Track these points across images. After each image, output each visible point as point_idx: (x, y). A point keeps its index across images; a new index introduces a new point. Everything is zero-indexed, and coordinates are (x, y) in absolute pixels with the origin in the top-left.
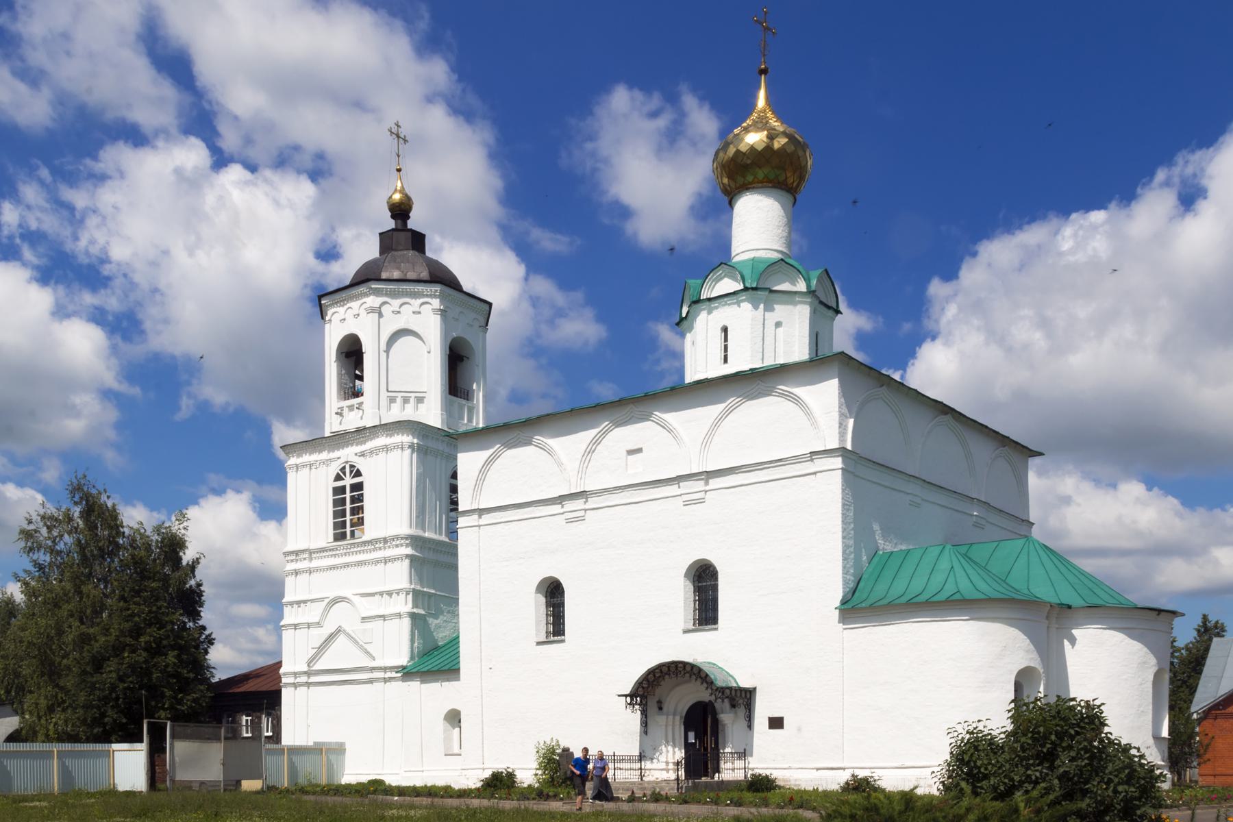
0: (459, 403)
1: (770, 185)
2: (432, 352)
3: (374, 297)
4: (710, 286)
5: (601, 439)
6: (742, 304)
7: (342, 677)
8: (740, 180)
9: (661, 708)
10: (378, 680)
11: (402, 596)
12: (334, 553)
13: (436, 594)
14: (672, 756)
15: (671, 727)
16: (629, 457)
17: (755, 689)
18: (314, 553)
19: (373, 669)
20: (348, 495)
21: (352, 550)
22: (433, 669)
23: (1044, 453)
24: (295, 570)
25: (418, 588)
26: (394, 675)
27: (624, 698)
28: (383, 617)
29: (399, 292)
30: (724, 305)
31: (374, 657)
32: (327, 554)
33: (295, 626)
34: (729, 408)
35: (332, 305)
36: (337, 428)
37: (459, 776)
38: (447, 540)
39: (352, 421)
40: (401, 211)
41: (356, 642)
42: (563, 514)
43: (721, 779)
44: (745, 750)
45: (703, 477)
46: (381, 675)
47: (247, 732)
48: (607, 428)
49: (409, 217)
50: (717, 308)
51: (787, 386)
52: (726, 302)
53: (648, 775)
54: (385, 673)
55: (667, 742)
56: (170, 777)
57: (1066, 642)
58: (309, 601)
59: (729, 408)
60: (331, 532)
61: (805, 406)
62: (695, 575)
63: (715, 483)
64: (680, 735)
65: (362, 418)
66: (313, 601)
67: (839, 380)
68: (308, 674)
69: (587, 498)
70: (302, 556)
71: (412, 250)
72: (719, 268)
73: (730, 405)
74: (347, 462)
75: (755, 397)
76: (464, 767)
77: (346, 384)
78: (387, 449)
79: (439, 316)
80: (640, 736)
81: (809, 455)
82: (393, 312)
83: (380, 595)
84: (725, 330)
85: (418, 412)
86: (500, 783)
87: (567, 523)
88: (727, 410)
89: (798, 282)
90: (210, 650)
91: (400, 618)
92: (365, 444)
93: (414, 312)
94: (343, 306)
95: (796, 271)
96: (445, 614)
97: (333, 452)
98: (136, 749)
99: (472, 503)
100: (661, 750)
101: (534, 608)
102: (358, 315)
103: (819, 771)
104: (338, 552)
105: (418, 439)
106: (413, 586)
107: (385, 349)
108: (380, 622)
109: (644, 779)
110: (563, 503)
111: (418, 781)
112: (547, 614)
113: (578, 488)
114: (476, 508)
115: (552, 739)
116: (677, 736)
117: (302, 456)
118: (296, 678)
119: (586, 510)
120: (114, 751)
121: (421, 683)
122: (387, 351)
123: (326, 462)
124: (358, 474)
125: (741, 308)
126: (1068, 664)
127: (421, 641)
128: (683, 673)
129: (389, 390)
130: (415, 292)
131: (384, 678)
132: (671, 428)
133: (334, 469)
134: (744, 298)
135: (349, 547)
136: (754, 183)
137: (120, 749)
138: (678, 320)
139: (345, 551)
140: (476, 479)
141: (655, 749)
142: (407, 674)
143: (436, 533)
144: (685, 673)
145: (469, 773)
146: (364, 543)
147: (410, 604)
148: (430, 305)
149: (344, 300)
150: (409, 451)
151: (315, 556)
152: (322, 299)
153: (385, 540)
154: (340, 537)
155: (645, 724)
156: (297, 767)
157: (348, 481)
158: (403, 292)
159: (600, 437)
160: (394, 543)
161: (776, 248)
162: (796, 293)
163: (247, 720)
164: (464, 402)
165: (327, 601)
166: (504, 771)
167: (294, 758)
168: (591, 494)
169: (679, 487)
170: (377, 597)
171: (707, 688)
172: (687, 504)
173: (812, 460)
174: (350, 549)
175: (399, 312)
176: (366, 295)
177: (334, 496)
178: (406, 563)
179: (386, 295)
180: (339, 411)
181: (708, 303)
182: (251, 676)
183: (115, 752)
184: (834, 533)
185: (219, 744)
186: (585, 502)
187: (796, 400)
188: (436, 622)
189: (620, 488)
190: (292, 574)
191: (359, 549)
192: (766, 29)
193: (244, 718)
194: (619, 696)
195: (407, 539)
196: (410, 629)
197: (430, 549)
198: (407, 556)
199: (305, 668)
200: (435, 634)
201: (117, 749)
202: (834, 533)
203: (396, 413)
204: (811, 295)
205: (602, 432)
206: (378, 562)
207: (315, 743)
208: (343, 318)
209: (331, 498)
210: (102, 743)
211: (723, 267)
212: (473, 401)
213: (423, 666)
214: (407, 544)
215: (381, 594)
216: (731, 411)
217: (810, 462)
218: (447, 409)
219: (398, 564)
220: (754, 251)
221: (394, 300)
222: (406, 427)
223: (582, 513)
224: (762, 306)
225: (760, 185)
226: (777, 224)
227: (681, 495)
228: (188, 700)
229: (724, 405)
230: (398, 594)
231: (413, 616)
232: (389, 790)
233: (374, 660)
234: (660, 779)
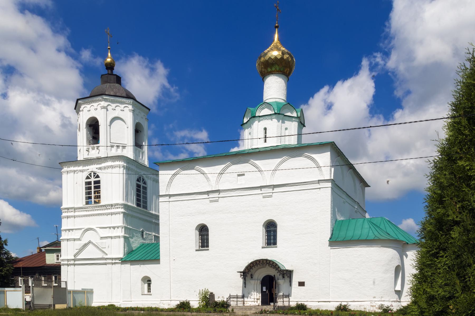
0: (139, 150)
1: (281, 73)
3: (105, 102)
4: (260, 111)
5: (226, 169)
6: (273, 119)
8: (269, 70)
9: (252, 278)
10: (109, 263)
11: (120, 229)
12: (86, 209)
13: (132, 229)
14: (256, 296)
15: (256, 285)
16: (238, 177)
17: (293, 271)
18: (76, 209)
20: (93, 185)
21: (95, 209)
23: (370, 186)
24: (67, 216)
25: (126, 226)
26: (117, 261)
27: (240, 273)
28: (111, 237)
29: (115, 101)
30: (265, 119)
32: (83, 210)
33: (68, 240)
34: (284, 160)
35: (84, 104)
36: (86, 156)
37: (160, 303)
38: (136, 206)
39: (94, 154)
41: (98, 247)
42: (209, 198)
43: (284, 305)
44: (289, 294)
45: (272, 187)
46: (110, 261)
47: (21, 284)
48: (229, 165)
50: (262, 120)
51: (308, 153)
52: (266, 118)
53: (246, 304)
54: (112, 260)
55: (254, 290)
56: (32, 302)
57: (404, 257)
58: (74, 229)
59: (284, 160)
60: (84, 201)
61: (316, 162)
62: (266, 226)
63: (276, 190)
64: (259, 289)
65: (99, 153)
67: (330, 153)
68: (74, 260)
69: (220, 193)
71: (117, 83)
72: (264, 104)
73: (284, 159)
74: (92, 172)
75: (295, 156)
76: (162, 300)
77: (89, 138)
78: (112, 167)
79: (132, 113)
80: (243, 288)
81: (318, 181)
82: (112, 109)
83: (109, 228)
84: (265, 129)
85: (123, 153)
86: (184, 306)
87: (210, 202)
88: (283, 161)
89: (294, 113)
91: (119, 238)
92: (101, 164)
93: (121, 110)
94: (89, 104)
95: (293, 108)
96: (135, 237)
97: (85, 166)
98: (17, 290)
100: (252, 293)
101: (194, 237)
102: (97, 109)
103: (319, 303)
104: (88, 209)
105: (126, 164)
106: (124, 225)
107: (109, 125)
108: (109, 240)
109: (245, 305)
110: (209, 194)
111: (128, 305)
112: (199, 239)
113: (216, 188)
114: (168, 194)
115: (205, 289)
116: (258, 289)
117: (70, 168)
118: (68, 262)
119: (219, 197)
120: (6, 291)
121: (131, 265)
122: (110, 126)
123: (82, 171)
124: (98, 177)
125: (273, 121)
126: (405, 264)
127: (128, 248)
128: (265, 264)
129: (111, 142)
130: (122, 101)
131: (112, 263)
132: (258, 166)
133: (86, 174)
134: (274, 117)
135: (90, 208)
136: (275, 71)
137: (9, 290)
138: (242, 124)
139: (92, 209)
140: (168, 182)
141: (249, 293)
142: (123, 261)
143: (132, 204)
144: (266, 264)
145: (164, 302)
146: (102, 206)
147: (123, 233)
148: (128, 108)
149: (89, 102)
150: (123, 168)
151: (77, 210)
152: (79, 100)
153: (112, 205)
154: (87, 203)
155: (245, 283)
156: (75, 299)
157: (93, 180)
158: (117, 101)
159: (226, 168)
160: (116, 207)
161: (282, 98)
162: (293, 117)
164: (140, 150)
166: (185, 301)
167: (75, 295)
168: (221, 191)
169: (261, 190)
170: (108, 229)
172: (264, 197)
173: (319, 183)
174: (94, 208)
175: (115, 110)
176: (100, 101)
177: (85, 185)
178: (122, 215)
179: (110, 102)
180: (87, 149)
181: (259, 118)
182: (17, 260)
183: (7, 292)
184: (327, 212)
186: (219, 194)
187: (313, 160)
188: (132, 240)
189: (235, 189)
190: (66, 218)
191: (99, 208)
192: (278, 10)
193: (20, 278)
194: (238, 272)
195: (122, 205)
196: (124, 243)
197: (130, 210)
198: (122, 212)
199: (73, 258)
200: (132, 245)
201: (8, 290)
202: (327, 212)
203: (114, 152)
204: (298, 119)
205: (227, 166)
206: (108, 214)
207: (82, 289)
208: (96, 108)
209: (84, 186)
210: (1, 288)
211: (265, 104)
212: (143, 149)
214: (122, 207)
215: (110, 228)
216: (284, 162)
217: (318, 184)
218: (135, 152)
220: (275, 99)
221: (113, 104)
222: (122, 158)
223: (217, 199)
224: (281, 121)
225: (277, 72)
226: (283, 89)
227: (262, 194)
228: (4, 270)
229: (281, 159)
230: (118, 228)
231: (125, 237)
232: (118, 309)
233: (107, 255)
234: (252, 305)
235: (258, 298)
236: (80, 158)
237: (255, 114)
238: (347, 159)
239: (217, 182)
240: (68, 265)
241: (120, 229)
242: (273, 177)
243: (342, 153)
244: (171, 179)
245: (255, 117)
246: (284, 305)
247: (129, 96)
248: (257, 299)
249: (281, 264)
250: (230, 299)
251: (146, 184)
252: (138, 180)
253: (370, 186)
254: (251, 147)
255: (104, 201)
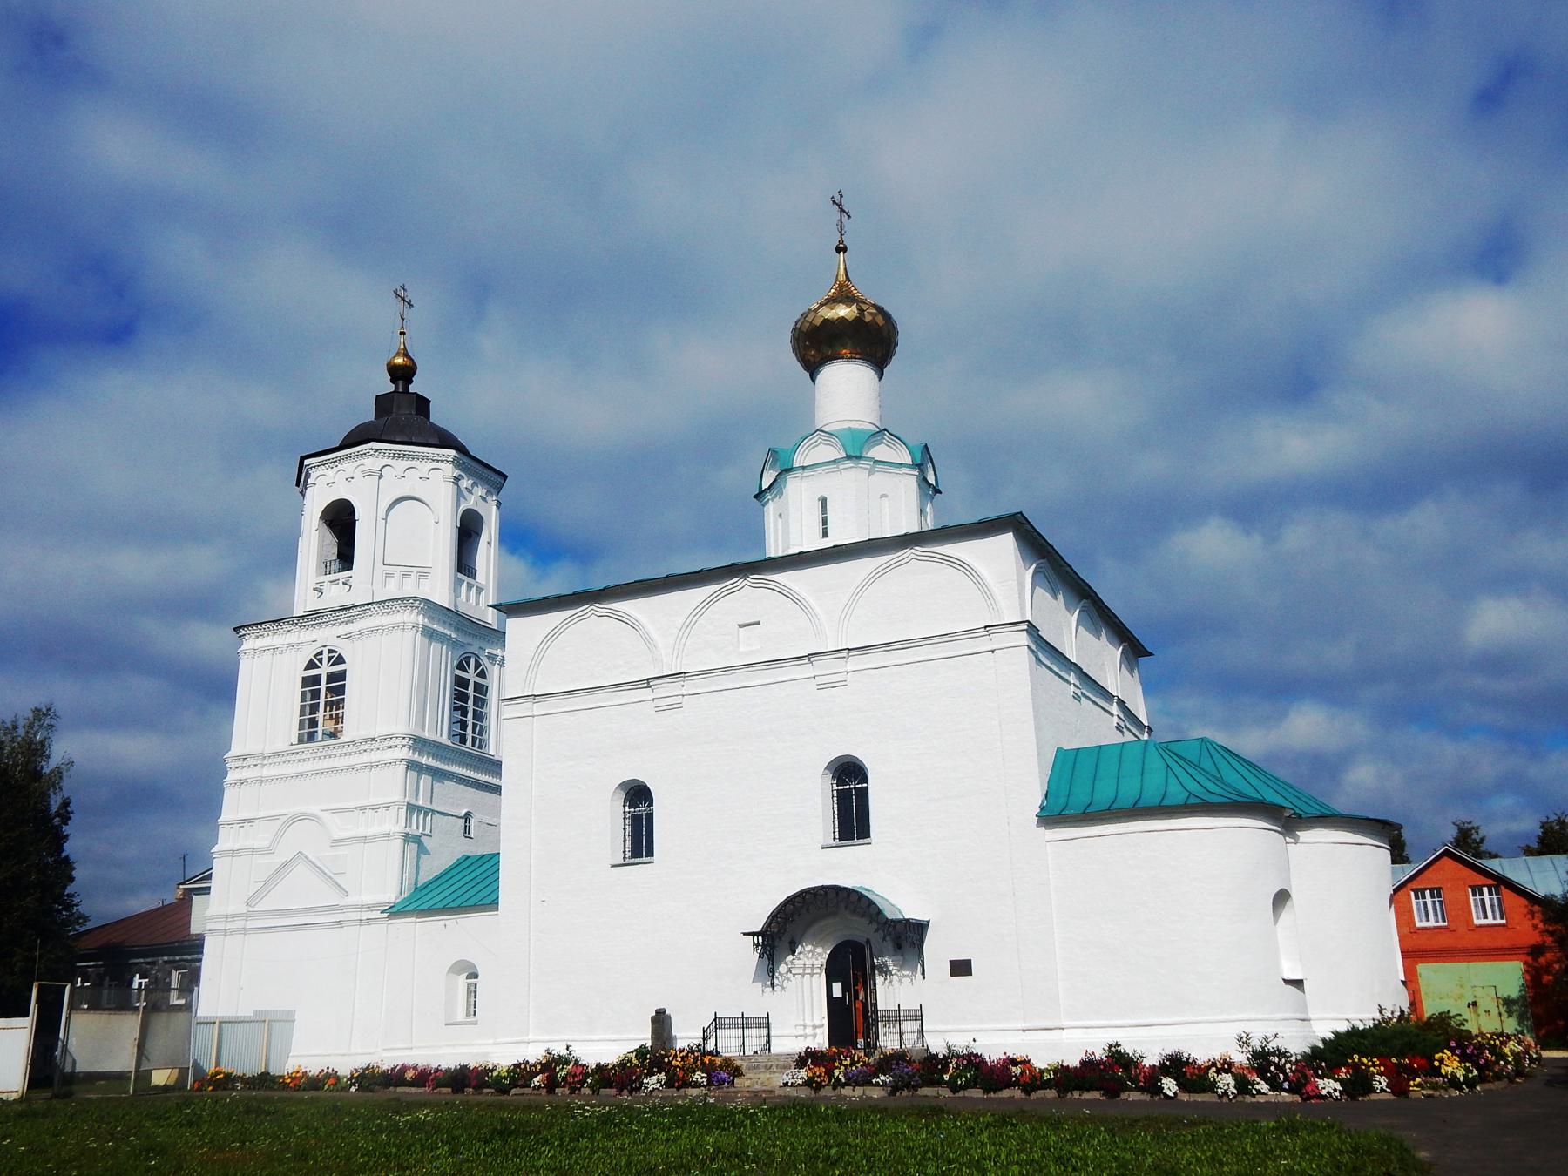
2: (441, 522)
5: (703, 610)
7: (304, 920)
11: (393, 811)
12: (298, 757)
19: (343, 909)
20: (323, 686)
22: (452, 905)
27: (751, 937)
31: (347, 892)
32: (275, 760)
39: (336, 595)
40: (402, 374)
43: (903, 1047)
46: (355, 916)
49: (412, 382)
61: (974, 574)
66: (261, 819)
68: (245, 916)
70: (251, 762)
84: (824, 501)
90: (1039, 810)
99: (524, 688)
101: (612, 820)
124: (340, 660)
133: (308, 654)
157: (324, 670)
163: (140, 984)
165: (283, 819)
171: (871, 922)
180: (318, 586)
185: (134, 1016)
194: (745, 934)
199: (243, 909)
203: (392, 590)
213: (420, 902)
215: (363, 809)
219: (388, 770)
223: (679, 699)
235: (818, 1023)
236: (298, 612)
237: (790, 464)
238: (1071, 567)
239: (676, 651)
240: (225, 932)
241: (393, 811)
242: (845, 626)
243: (1052, 547)
244: (539, 650)
245: (788, 470)
246: (710, 1047)
247: (444, 440)
248: (815, 1027)
249: (887, 900)
250: (716, 1032)
251: (485, 677)
252: (461, 667)
253: (1151, 654)
254: (784, 551)
255: (350, 730)
